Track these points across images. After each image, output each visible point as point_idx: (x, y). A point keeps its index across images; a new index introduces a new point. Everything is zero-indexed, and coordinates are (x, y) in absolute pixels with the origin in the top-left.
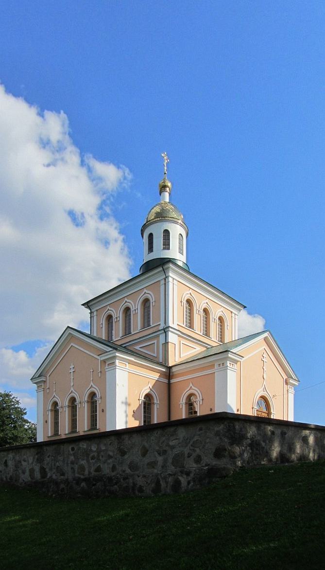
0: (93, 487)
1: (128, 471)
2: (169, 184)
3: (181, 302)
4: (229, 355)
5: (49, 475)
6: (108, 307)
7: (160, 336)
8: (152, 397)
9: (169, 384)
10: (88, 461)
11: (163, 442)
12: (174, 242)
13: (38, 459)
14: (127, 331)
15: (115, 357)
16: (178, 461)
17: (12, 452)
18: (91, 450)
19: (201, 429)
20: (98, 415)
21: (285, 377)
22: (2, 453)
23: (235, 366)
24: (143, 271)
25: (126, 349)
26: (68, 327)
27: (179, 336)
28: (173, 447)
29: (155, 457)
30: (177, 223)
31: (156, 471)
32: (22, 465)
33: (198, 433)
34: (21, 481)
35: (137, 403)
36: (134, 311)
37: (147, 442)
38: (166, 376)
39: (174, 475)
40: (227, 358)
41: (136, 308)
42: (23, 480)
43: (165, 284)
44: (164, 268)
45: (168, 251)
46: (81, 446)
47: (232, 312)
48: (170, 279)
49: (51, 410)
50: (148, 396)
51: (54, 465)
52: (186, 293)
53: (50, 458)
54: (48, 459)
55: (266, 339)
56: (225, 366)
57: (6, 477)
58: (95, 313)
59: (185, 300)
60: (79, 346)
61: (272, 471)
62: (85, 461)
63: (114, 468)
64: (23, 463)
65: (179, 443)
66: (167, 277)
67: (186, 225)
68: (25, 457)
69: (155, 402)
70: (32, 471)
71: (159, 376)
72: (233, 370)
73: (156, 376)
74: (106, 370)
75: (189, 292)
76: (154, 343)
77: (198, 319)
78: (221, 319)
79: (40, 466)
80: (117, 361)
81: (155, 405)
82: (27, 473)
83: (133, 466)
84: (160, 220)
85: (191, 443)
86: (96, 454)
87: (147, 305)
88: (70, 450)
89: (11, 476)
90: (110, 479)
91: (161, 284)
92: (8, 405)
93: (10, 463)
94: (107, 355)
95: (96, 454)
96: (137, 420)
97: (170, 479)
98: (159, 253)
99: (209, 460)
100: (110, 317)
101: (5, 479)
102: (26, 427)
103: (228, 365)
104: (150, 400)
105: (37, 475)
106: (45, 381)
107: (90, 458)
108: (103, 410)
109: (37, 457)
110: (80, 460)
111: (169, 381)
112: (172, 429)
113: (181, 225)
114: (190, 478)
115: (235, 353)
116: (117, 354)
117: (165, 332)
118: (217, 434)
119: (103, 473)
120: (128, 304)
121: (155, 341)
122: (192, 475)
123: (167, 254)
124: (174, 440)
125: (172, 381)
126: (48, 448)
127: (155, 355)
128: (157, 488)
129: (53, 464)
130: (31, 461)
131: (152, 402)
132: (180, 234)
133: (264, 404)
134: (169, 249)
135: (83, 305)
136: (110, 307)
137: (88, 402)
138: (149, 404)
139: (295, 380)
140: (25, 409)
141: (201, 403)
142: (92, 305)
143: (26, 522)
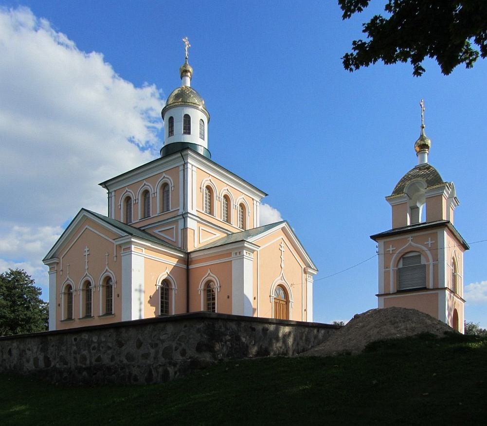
0: (94, 376)
1: (125, 361)
2: (191, 69)
3: (200, 188)
4: (245, 245)
5: (53, 364)
6: (145, 182)
7: (179, 222)
8: (170, 282)
9: (188, 270)
10: (90, 352)
11: (155, 336)
12: (195, 127)
13: (41, 348)
14: (146, 214)
15: (131, 243)
16: (167, 353)
17: (17, 341)
18: (92, 341)
19: (185, 326)
20: (113, 300)
21: (304, 266)
22: (6, 342)
23: (252, 255)
24: (163, 153)
25: (146, 233)
26: (83, 209)
27: (198, 222)
28: (163, 341)
29: (148, 348)
30: (197, 108)
31: (148, 362)
32: (26, 354)
33: (184, 329)
34: (25, 369)
35: (154, 288)
36: (173, 188)
37: (142, 336)
38: (185, 261)
39: (164, 365)
40: (244, 248)
41: (155, 191)
42: (28, 369)
43: (184, 170)
44: (182, 154)
45: (188, 136)
46: (83, 337)
47: (253, 199)
48: (189, 166)
49: (65, 293)
50: (166, 282)
51: (58, 355)
52: (206, 179)
53: (54, 347)
54: (52, 348)
55: (283, 229)
56: (242, 254)
57: (10, 366)
58: (113, 194)
59: (205, 187)
60: (93, 228)
61: (238, 365)
62: (87, 351)
63: (112, 359)
64: (27, 352)
65: (168, 338)
66: (185, 164)
67: (208, 110)
68: (30, 346)
69: (173, 287)
70: (36, 360)
71: (177, 262)
72: (248, 258)
73: (174, 262)
74: (122, 255)
75: (209, 179)
76: (173, 228)
77: (219, 206)
78: (242, 205)
79: (44, 355)
80: (133, 246)
81: (173, 291)
82: (32, 362)
83: (130, 357)
84: (181, 104)
85: (178, 338)
86: (96, 345)
87: (166, 189)
88: (73, 340)
89: (15, 365)
90: (109, 369)
91: (180, 169)
92: (21, 284)
93: (15, 352)
94: (122, 240)
95: (96, 345)
96: (154, 306)
97: (161, 370)
98: (180, 137)
99: (191, 352)
100: (128, 199)
101: (8, 368)
102: (40, 307)
103: (245, 254)
104: (167, 285)
105: (41, 364)
106: (58, 263)
107: (91, 349)
108: (118, 295)
109: (41, 346)
110: (82, 350)
111: (188, 267)
112: (162, 325)
113: (202, 111)
114: (176, 369)
115: (251, 243)
116: (132, 240)
117: (184, 218)
118: (198, 331)
119: (103, 363)
120: (167, 179)
121: (174, 226)
122: (178, 366)
123: (187, 139)
124: (164, 334)
125: (191, 267)
126: (52, 338)
127: (174, 240)
128: (149, 379)
129: (57, 353)
130: (35, 350)
131: (170, 287)
132: (201, 120)
133: (282, 292)
134: (189, 133)
135: (100, 184)
136: (129, 189)
137: (103, 286)
138: (167, 290)
139: (314, 269)
140: (40, 289)
141: (219, 290)
142: (109, 185)
143: (464, 345)
